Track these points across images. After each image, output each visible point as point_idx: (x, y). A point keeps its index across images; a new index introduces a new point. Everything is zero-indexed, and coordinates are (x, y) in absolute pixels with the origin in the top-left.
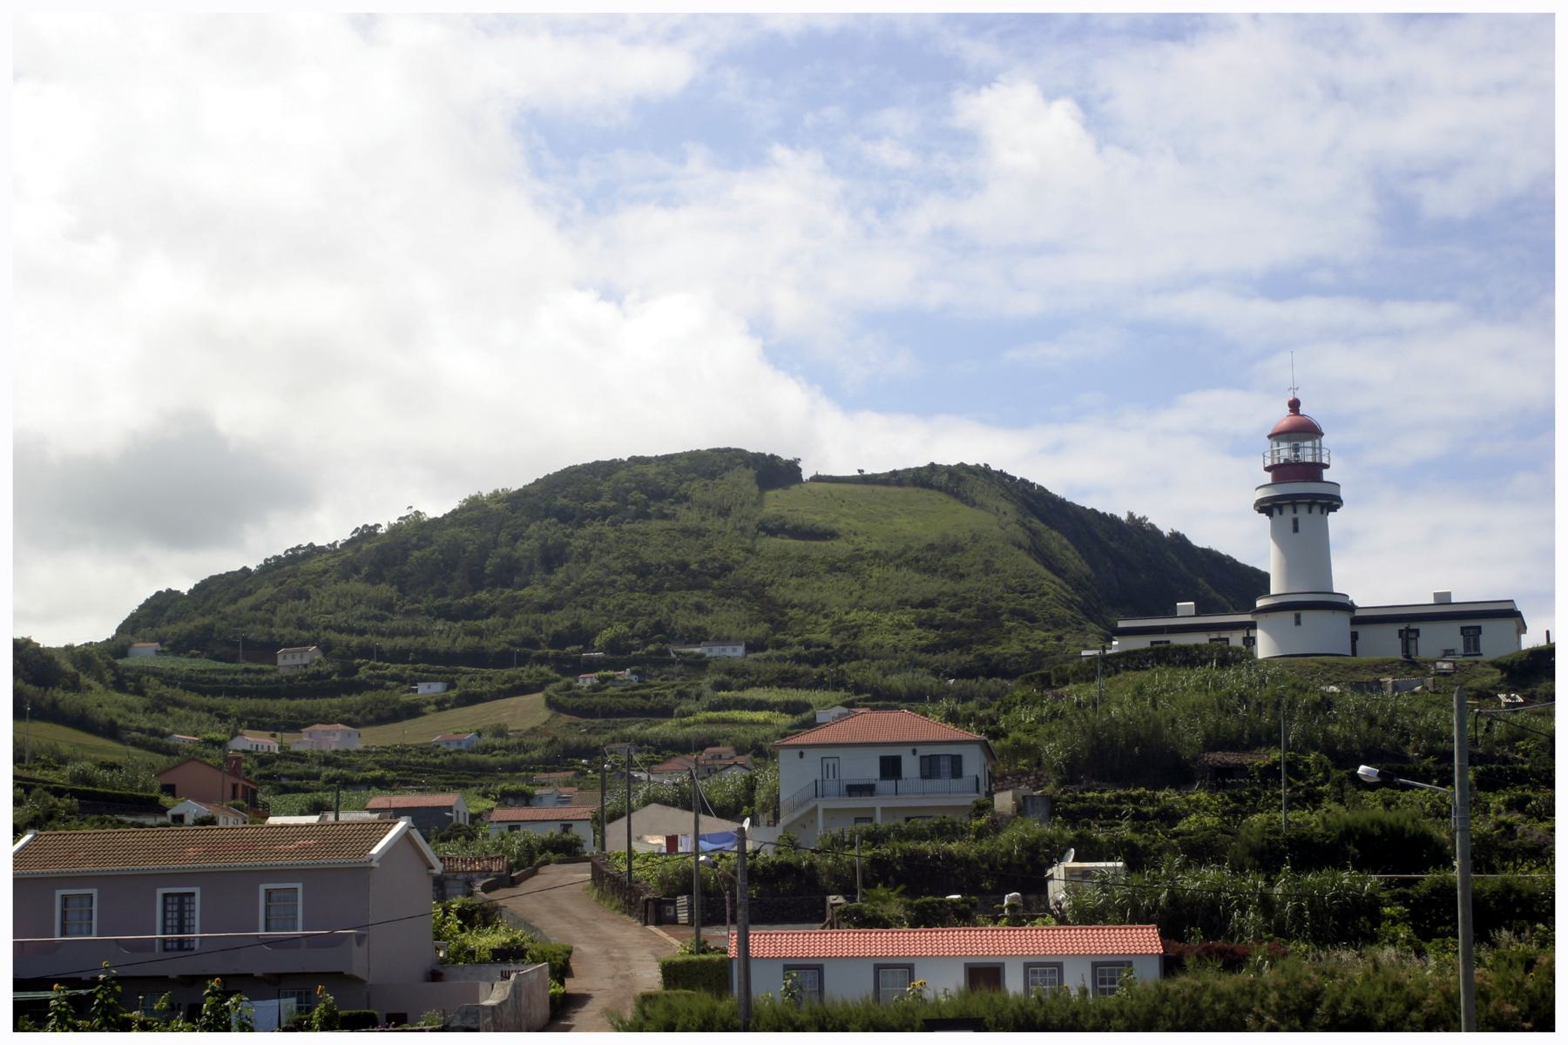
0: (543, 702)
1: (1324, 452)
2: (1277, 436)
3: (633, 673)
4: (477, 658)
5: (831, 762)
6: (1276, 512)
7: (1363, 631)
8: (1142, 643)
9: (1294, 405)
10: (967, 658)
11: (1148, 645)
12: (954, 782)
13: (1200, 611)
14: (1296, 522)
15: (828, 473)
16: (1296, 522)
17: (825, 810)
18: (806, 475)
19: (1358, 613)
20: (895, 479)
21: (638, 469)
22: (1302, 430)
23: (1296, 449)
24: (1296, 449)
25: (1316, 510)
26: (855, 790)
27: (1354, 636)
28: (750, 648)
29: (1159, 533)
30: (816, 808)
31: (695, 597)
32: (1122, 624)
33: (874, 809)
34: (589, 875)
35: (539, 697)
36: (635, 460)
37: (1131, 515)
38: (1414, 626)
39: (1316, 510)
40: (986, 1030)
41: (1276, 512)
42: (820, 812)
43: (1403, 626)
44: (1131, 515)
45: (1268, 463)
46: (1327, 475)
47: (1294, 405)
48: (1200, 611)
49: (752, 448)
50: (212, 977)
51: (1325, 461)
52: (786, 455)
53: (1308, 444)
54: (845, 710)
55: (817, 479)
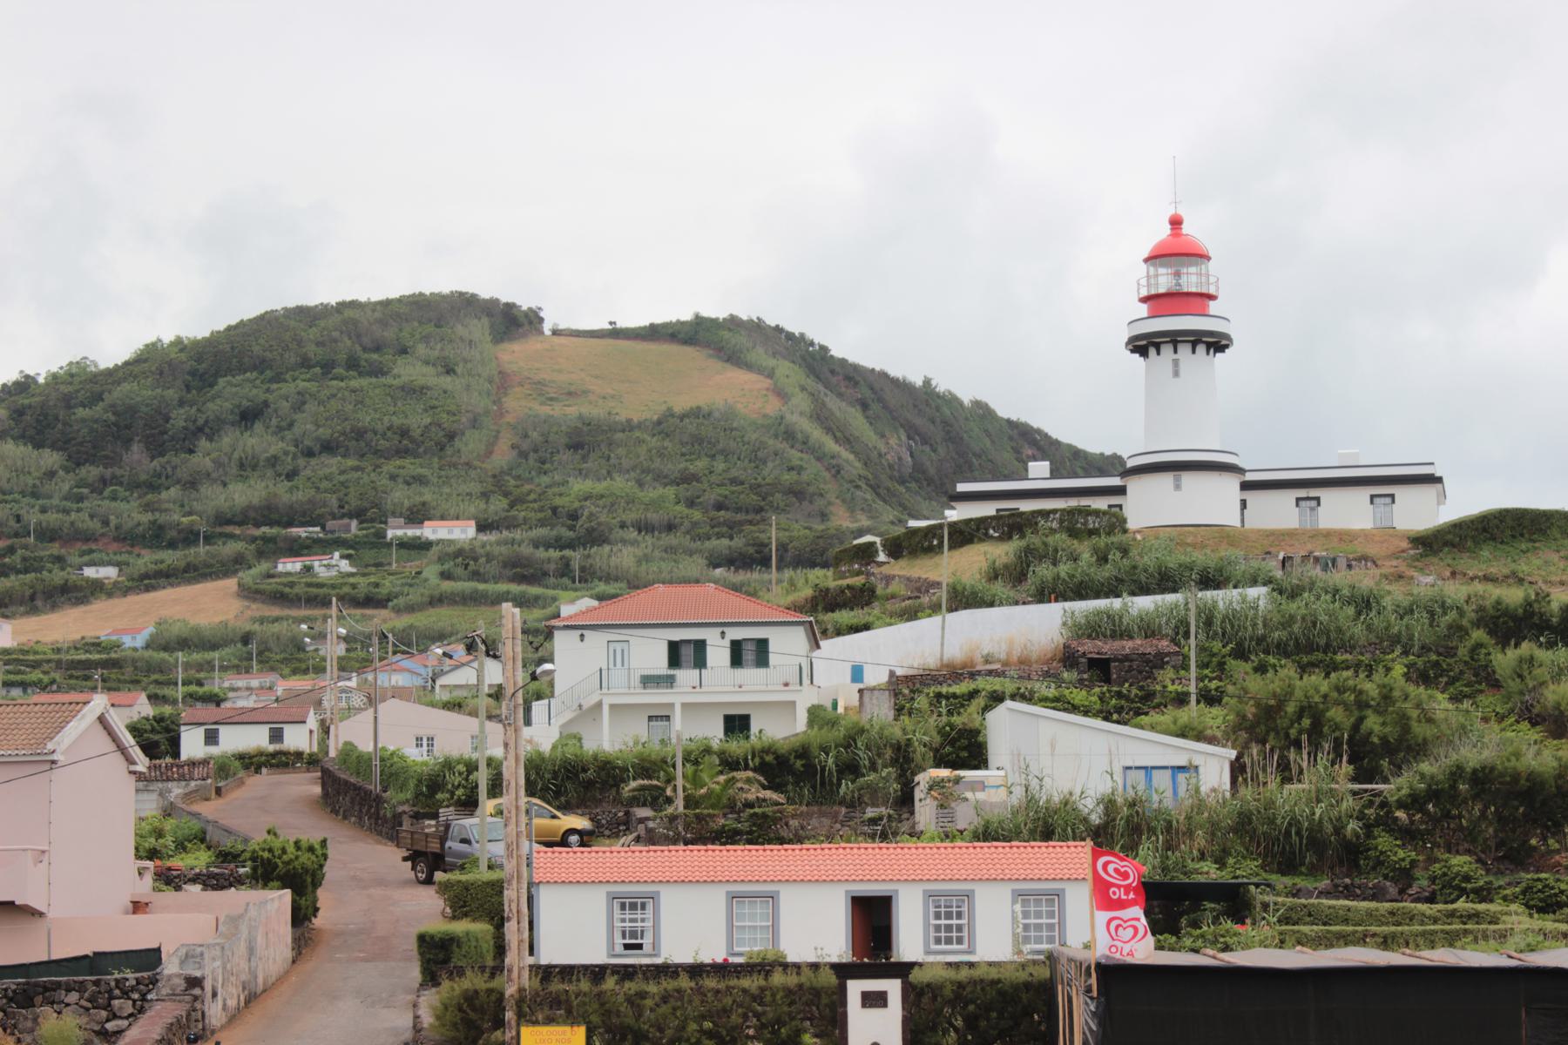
0: (235, 588)
1: (1212, 280)
2: (1154, 258)
3: (342, 557)
4: (157, 536)
5: (619, 647)
6: (1152, 351)
7: (1253, 497)
8: (987, 509)
9: (1176, 222)
10: (738, 543)
11: (992, 512)
12: (762, 671)
13: (1055, 474)
14: (1176, 363)
15: (574, 327)
16: (1176, 363)
17: (612, 707)
18: (547, 328)
19: (1249, 477)
20: (654, 333)
21: (348, 313)
22: (1176, 251)
23: (1177, 274)
24: (1177, 274)
25: (1201, 349)
26: (648, 681)
27: (1244, 504)
28: (482, 528)
29: (961, 403)
30: (599, 705)
31: (410, 466)
32: (962, 487)
33: (672, 705)
34: (318, 790)
35: (231, 584)
36: (343, 306)
37: (927, 382)
38: (1313, 493)
39: (1201, 349)
40: (586, 967)
41: (1152, 351)
42: (606, 709)
43: (1302, 493)
44: (927, 382)
45: (1144, 293)
46: (1213, 307)
47: (1176, 222)
48: (1055, 474)
49: (485, 293)
50: (233, 1018)
51: (1212, 291)
52: (525, 303)
53: (1193, 270)
54: (595, 603)
55: (556, 332)
